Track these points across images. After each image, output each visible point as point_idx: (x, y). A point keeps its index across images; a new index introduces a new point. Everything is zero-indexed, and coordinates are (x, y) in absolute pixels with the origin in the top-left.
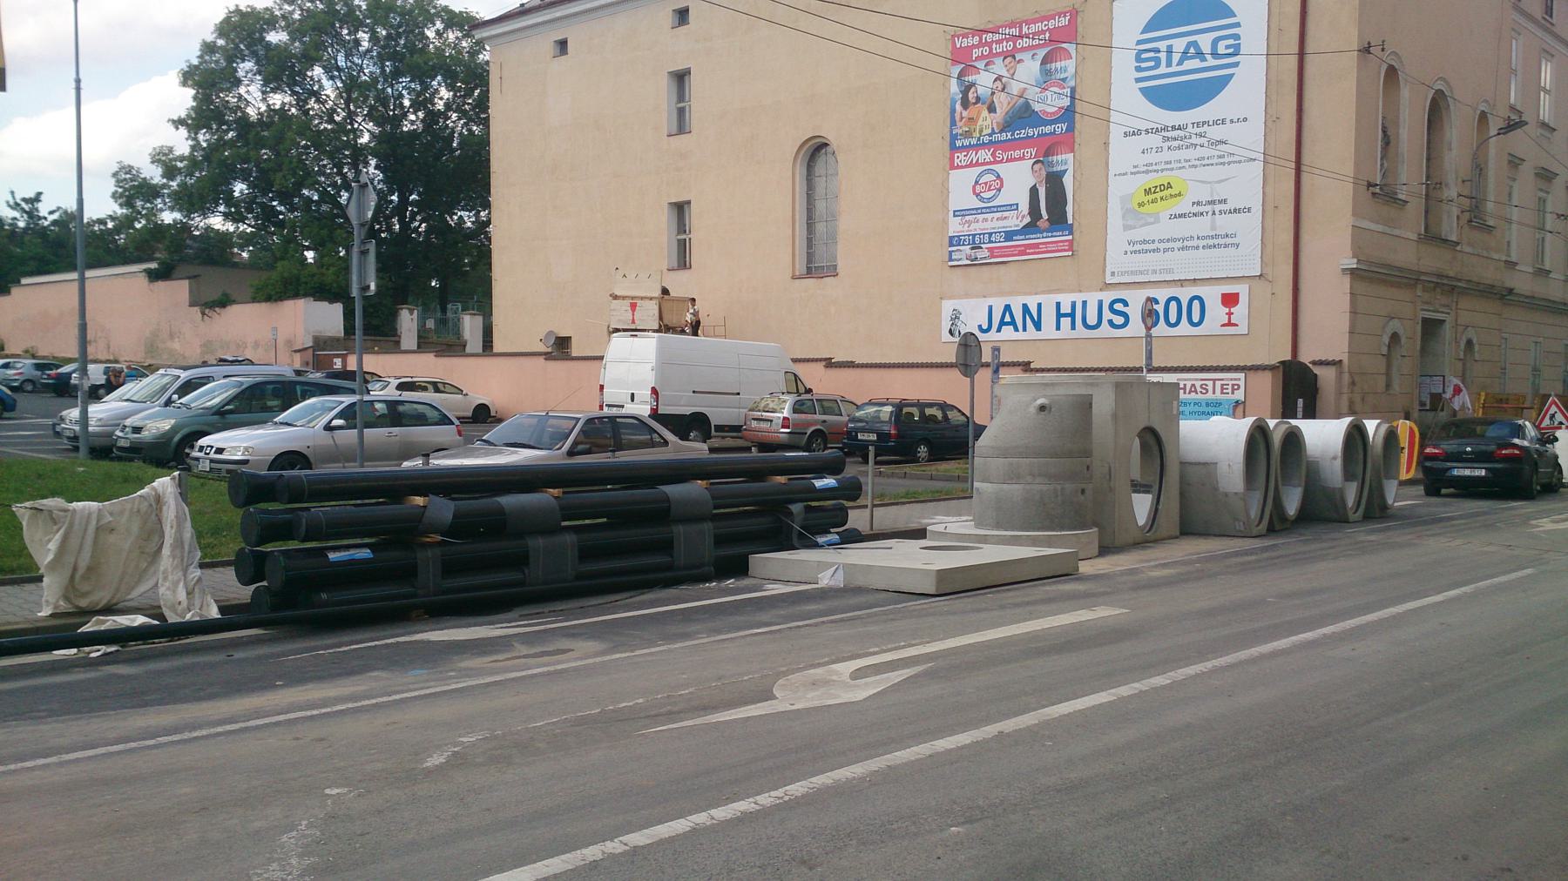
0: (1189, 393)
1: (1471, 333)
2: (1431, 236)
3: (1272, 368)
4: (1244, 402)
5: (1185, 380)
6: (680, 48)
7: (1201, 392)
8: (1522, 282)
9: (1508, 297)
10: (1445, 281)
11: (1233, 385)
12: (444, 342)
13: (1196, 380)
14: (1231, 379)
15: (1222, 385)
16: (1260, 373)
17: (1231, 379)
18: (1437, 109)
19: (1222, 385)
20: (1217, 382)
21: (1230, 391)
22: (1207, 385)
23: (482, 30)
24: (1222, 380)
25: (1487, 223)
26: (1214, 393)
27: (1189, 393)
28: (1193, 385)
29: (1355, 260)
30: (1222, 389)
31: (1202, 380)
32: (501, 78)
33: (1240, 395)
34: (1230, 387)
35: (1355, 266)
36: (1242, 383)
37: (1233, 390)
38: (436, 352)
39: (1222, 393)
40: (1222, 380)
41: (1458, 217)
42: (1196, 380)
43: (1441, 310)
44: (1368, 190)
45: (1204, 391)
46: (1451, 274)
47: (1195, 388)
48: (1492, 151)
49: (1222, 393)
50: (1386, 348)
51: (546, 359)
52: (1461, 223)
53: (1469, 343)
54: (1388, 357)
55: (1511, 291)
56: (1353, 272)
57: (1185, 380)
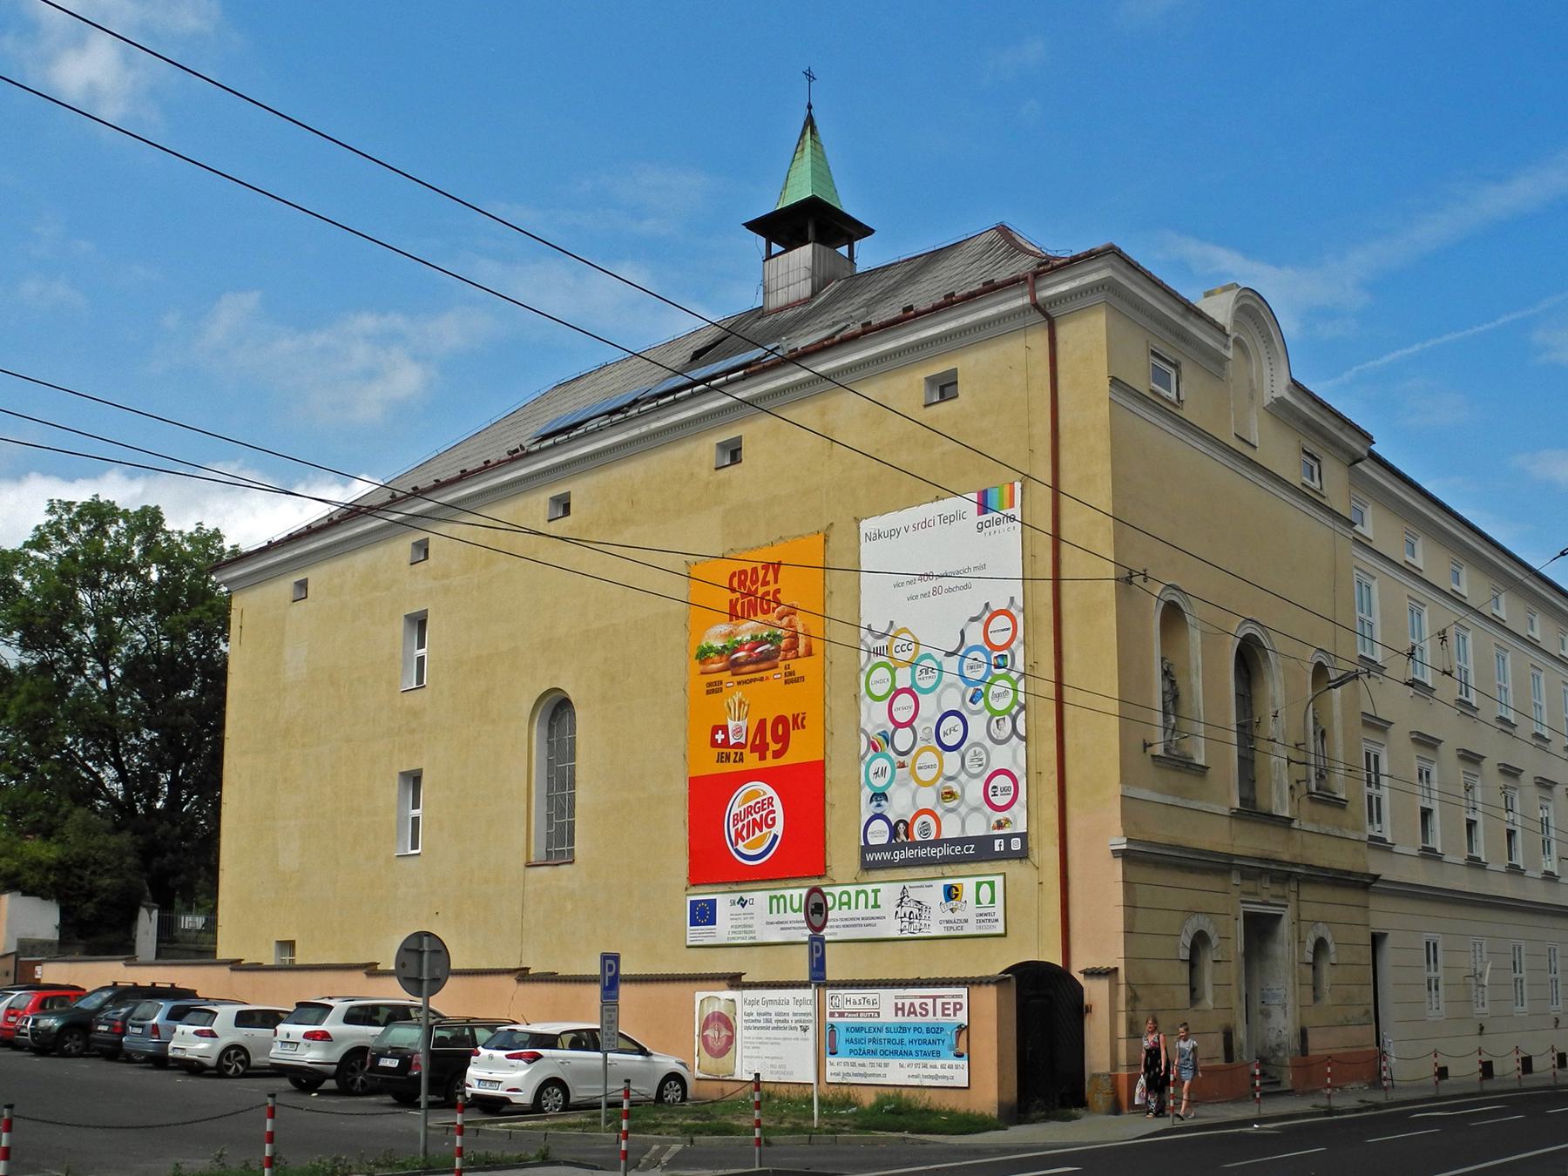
0: (908, 1015)
1: (1322, 931)
2: (1251, 811)
3: (998, 981)
4: (967, 1027)
5: (903, 997)
6: (417, 589)
7: (921, 1013)
8: (1402, 869)
9: (1374, 885)
10: (1273, 867)
11: (955, 1004)
12: (172, 947)
13: (915, 997)
14: (953, 997)
15: (943, 1004)
16: (983, 988)
17: (953, 997)
18: (1249, 658)
19: (943, 1004)
20: (937, 1000)
21: (951, 1012)
22: (926, 1005)
23: (223, 572)
24: (943, 997)
25: (1337, 796)
26: (935, 1015)
27: (908, 1015)
28: (912, 1005)
29: (1125, 840)
30: (944, 1009)
31: (922, 997)
32: (241, 627)
33: (962, 1018)
34: (951, 1007)
35: (1124, 847)
36: (964, 1001)
37: (955, 1010)
38: (126, 959)
39: (944, 1015)
40: (943, 997)
41: (1291, 788)
42: (915, 997)
43: (1271, 902)
44: (1145, 751)
45: (924, 1013)
46: (1286, 857)
47: (914, 1008)
48: (1337, 710)
49: (944, 1015)
50: (1312, 956)
51: (232, 969)
52: (1297, 796)
53: (1320, 945)
54: (1315, 966)
55: (1376, 878)
56: (1125, 856)
57: (903, 997)
